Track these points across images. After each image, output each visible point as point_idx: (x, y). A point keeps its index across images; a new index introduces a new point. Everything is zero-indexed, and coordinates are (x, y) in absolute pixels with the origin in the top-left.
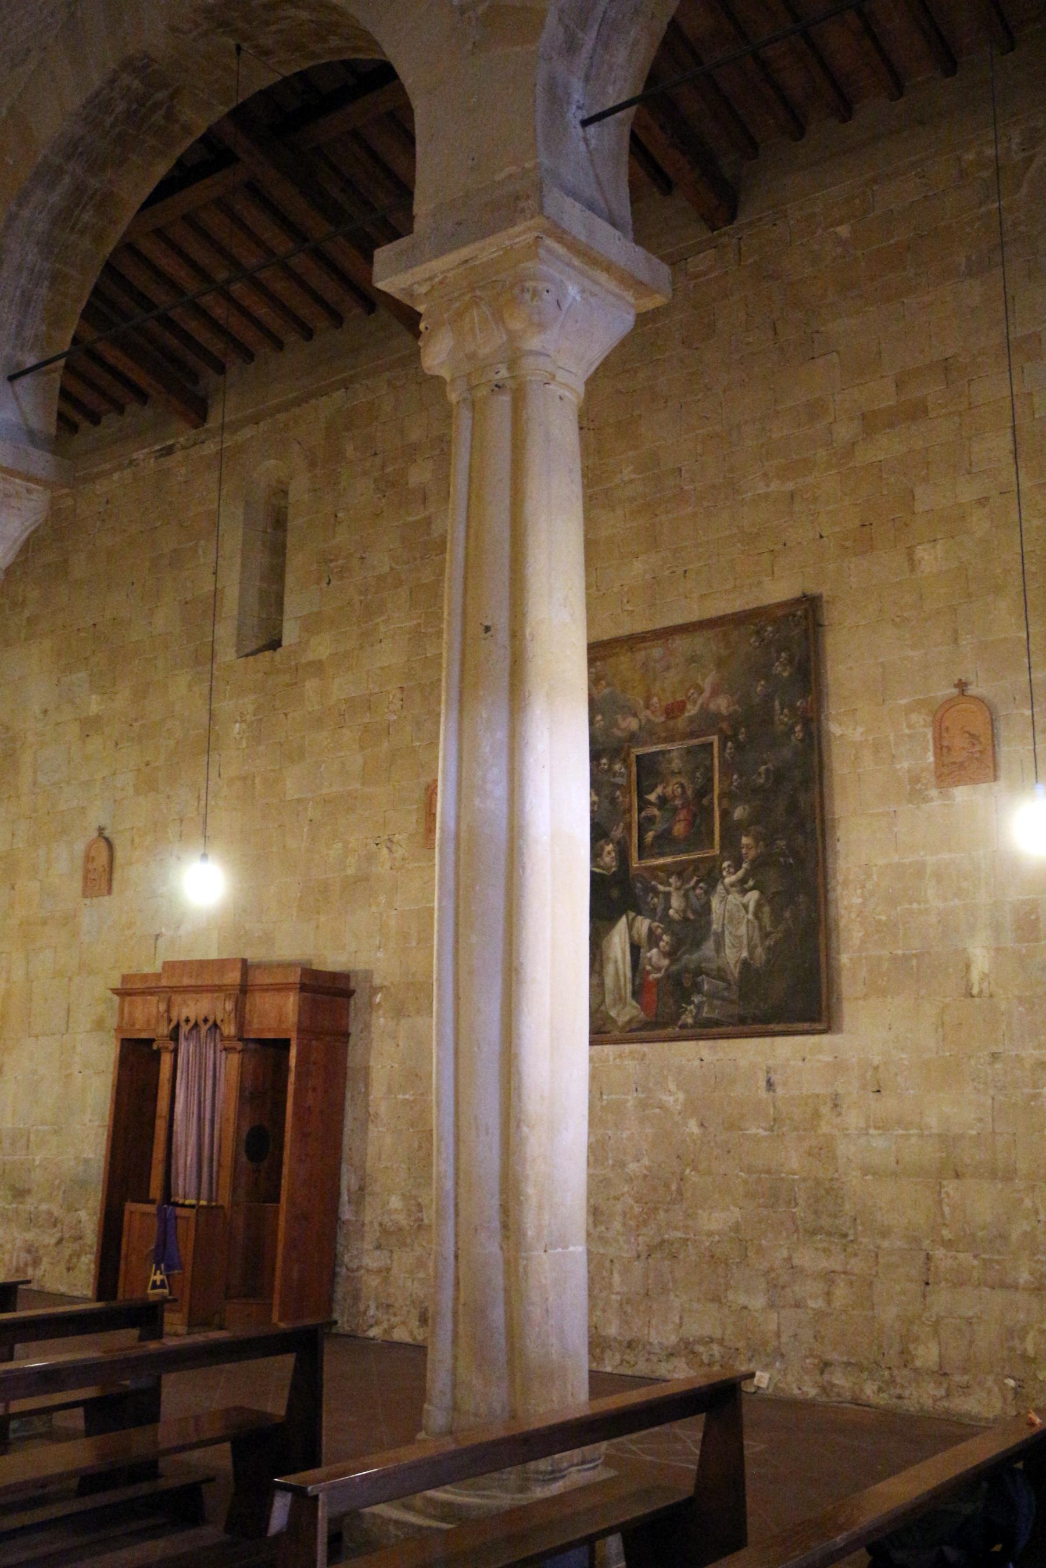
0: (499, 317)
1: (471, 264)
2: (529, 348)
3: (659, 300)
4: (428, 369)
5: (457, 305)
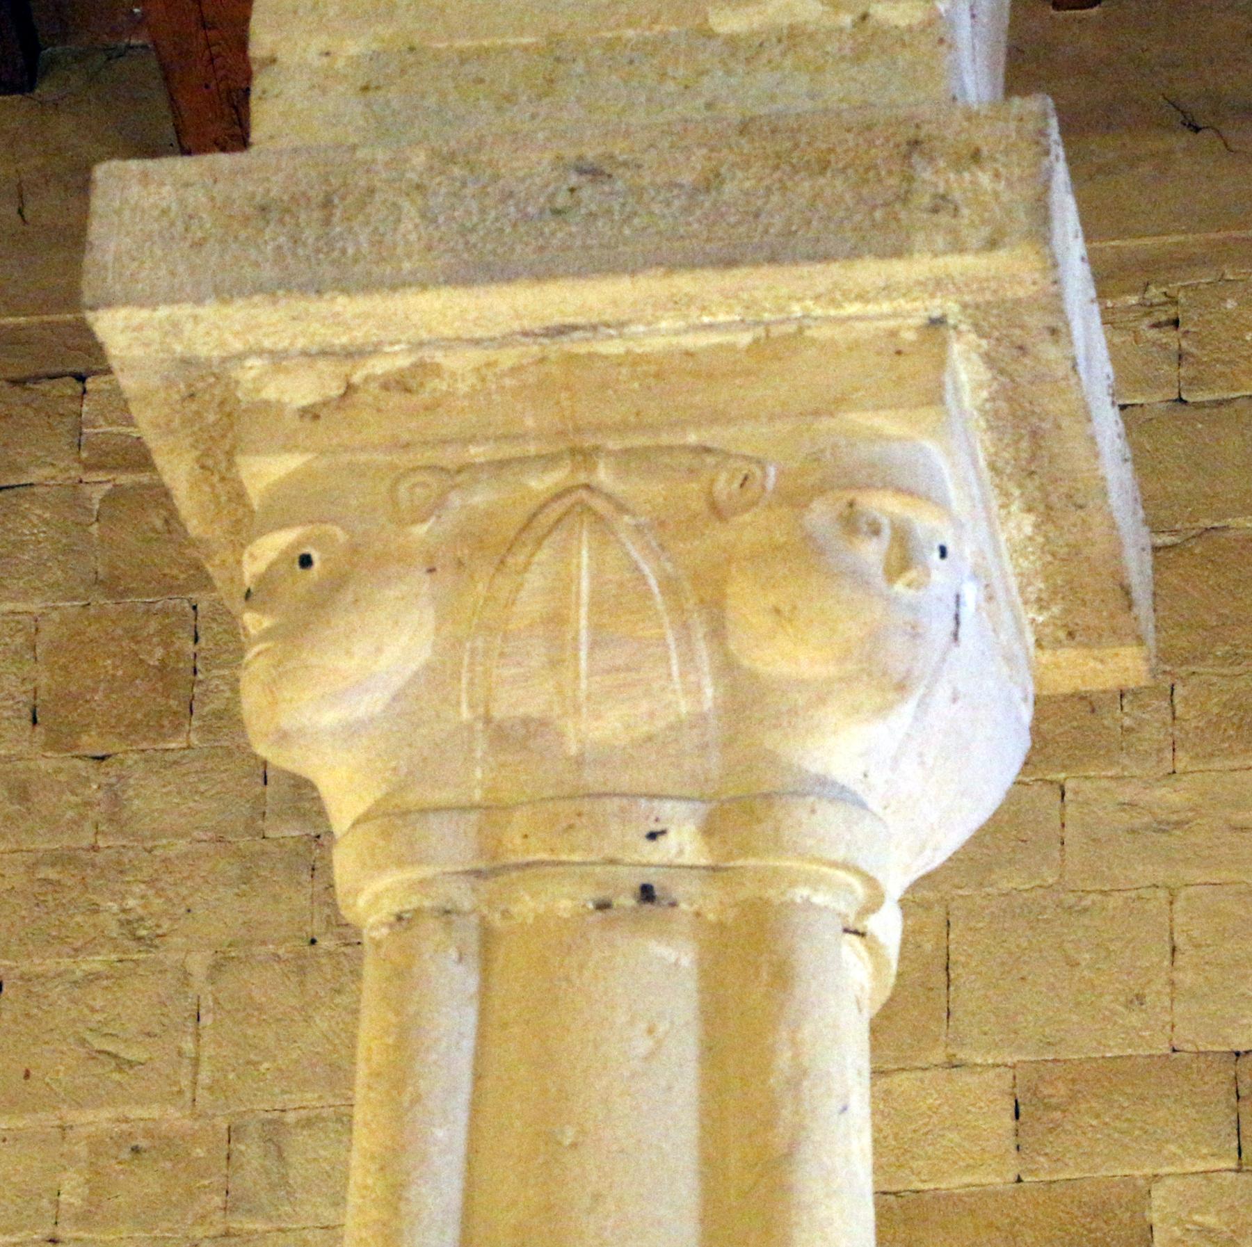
0: (705, 601)
1: (577, 345)
2: (815, 768)
3: (1126, 665)
4: (284, 737)
5: (482, 497)
